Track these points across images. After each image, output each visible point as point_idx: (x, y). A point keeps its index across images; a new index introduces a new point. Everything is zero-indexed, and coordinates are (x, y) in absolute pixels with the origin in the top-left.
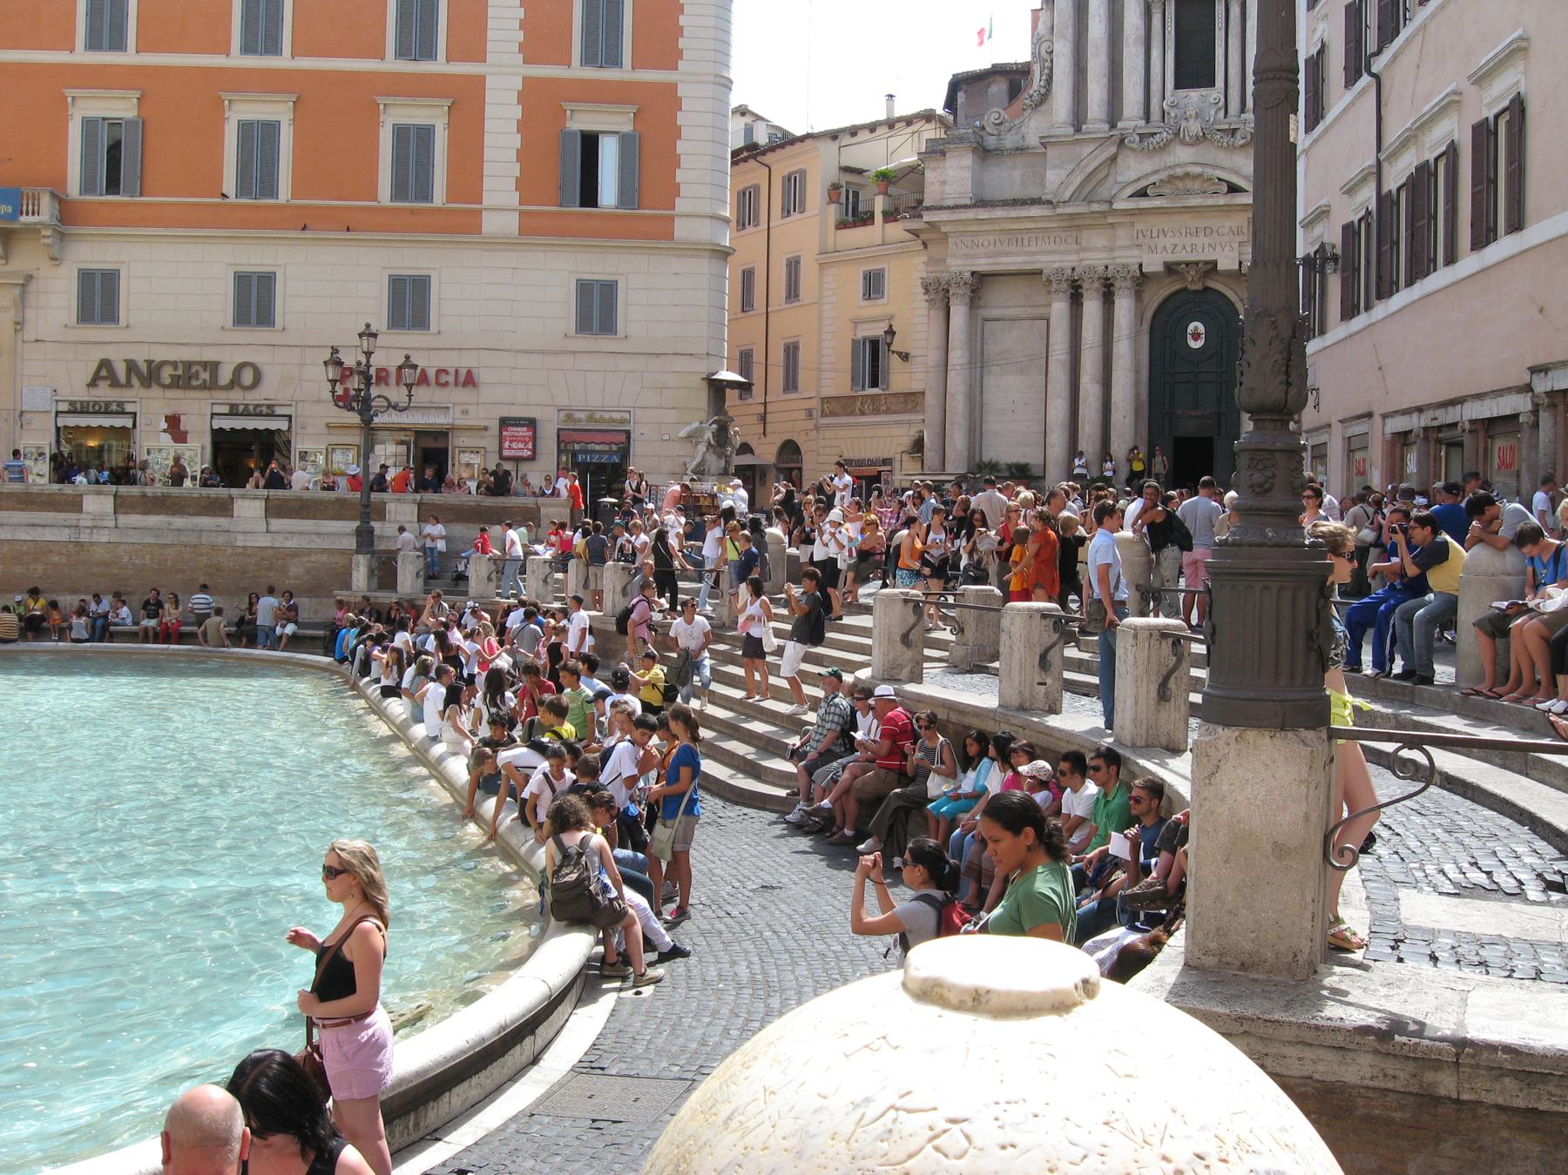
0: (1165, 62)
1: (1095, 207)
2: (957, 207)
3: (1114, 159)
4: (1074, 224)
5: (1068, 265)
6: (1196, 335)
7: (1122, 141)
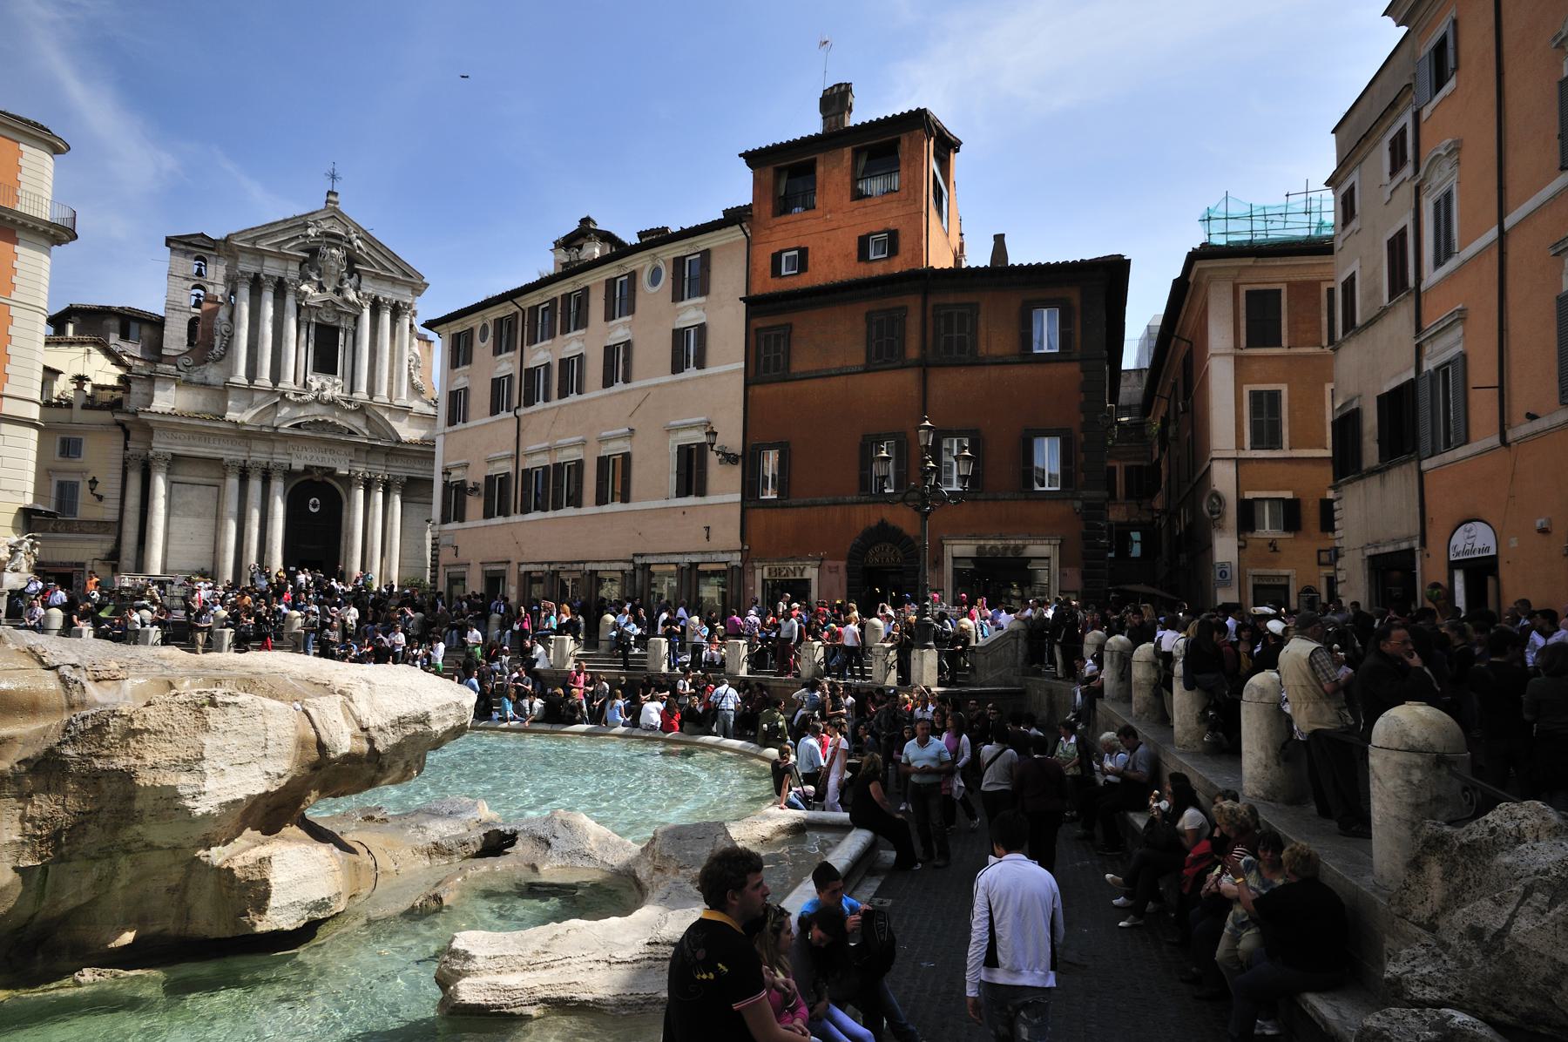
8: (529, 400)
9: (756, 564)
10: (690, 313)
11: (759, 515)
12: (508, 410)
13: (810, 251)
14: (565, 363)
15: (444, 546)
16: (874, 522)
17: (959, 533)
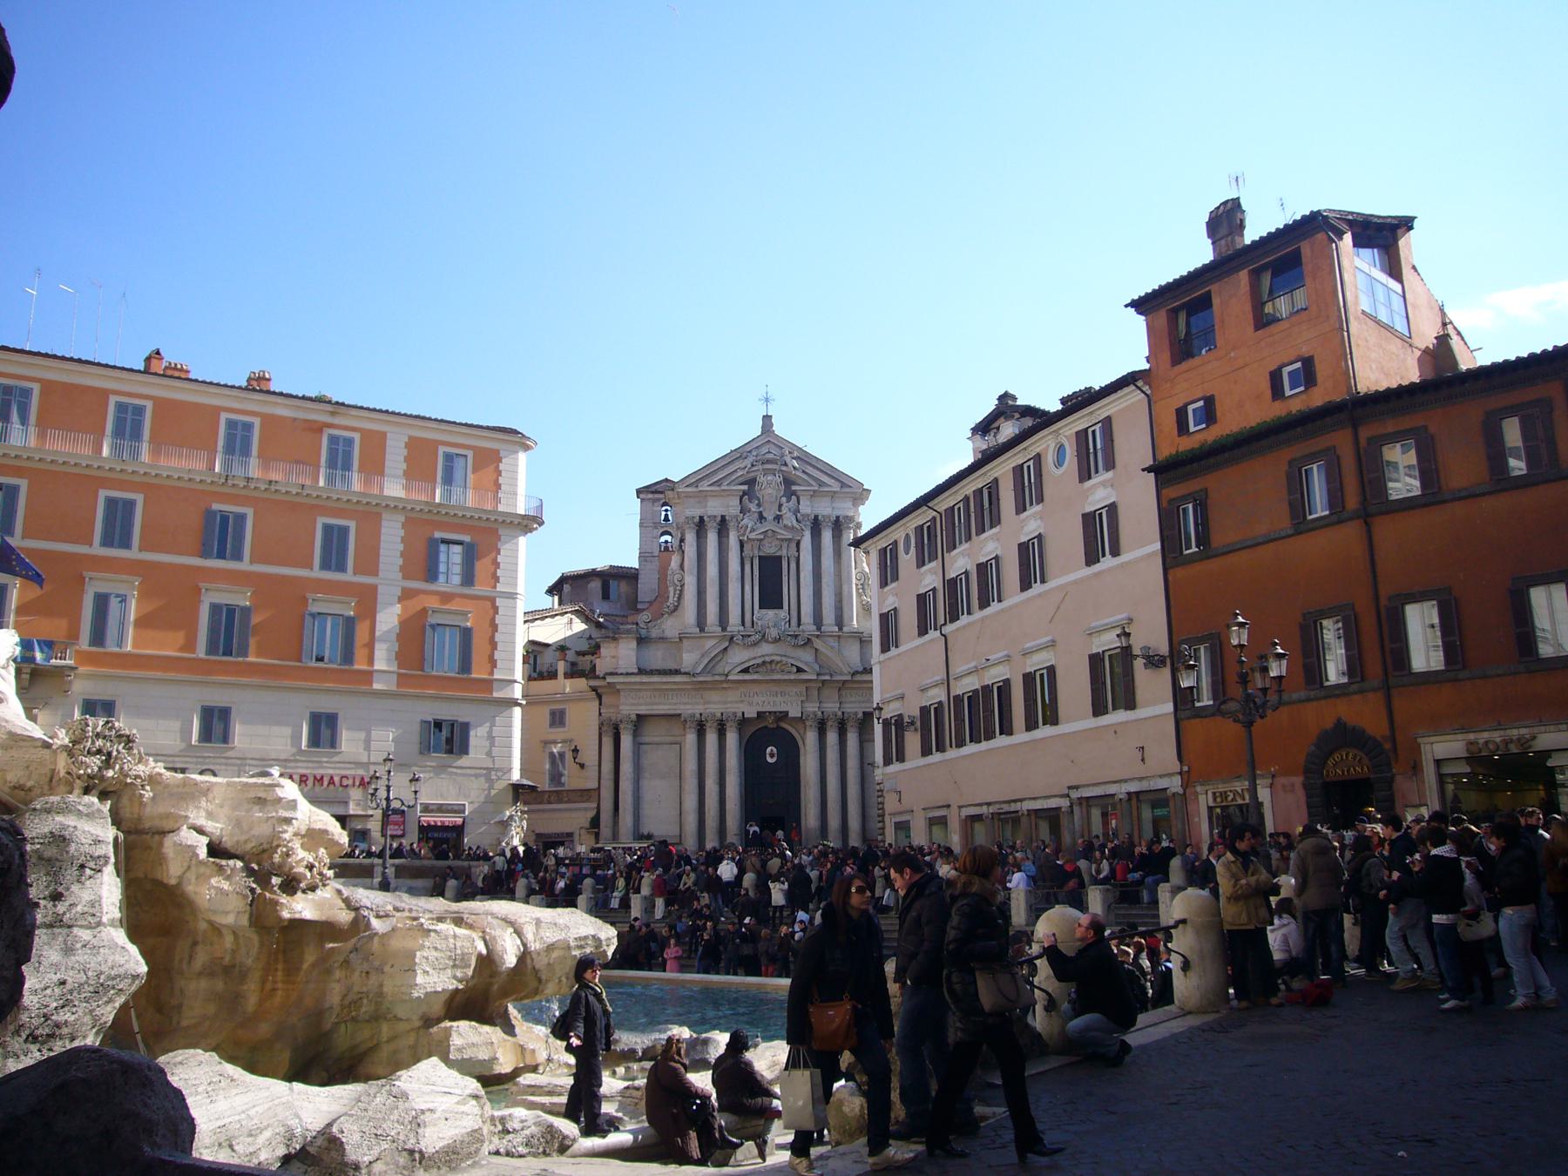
0: (753, 593)
1: (717, 678)
2: (627, 674)
3: (726, 649)
4: (702, 687)
5: (698, 712)
6: (771, 755)
7: (732, 638)
8: (953, 616)
9: (1199, 789)
10: (1098, 493)
11: (1195, 727)
12: (936, 629)
13: (1217, 398)
14: (982, 568)
15: (888, 791)
16: (1329, 724)
17: (1439, 724)
